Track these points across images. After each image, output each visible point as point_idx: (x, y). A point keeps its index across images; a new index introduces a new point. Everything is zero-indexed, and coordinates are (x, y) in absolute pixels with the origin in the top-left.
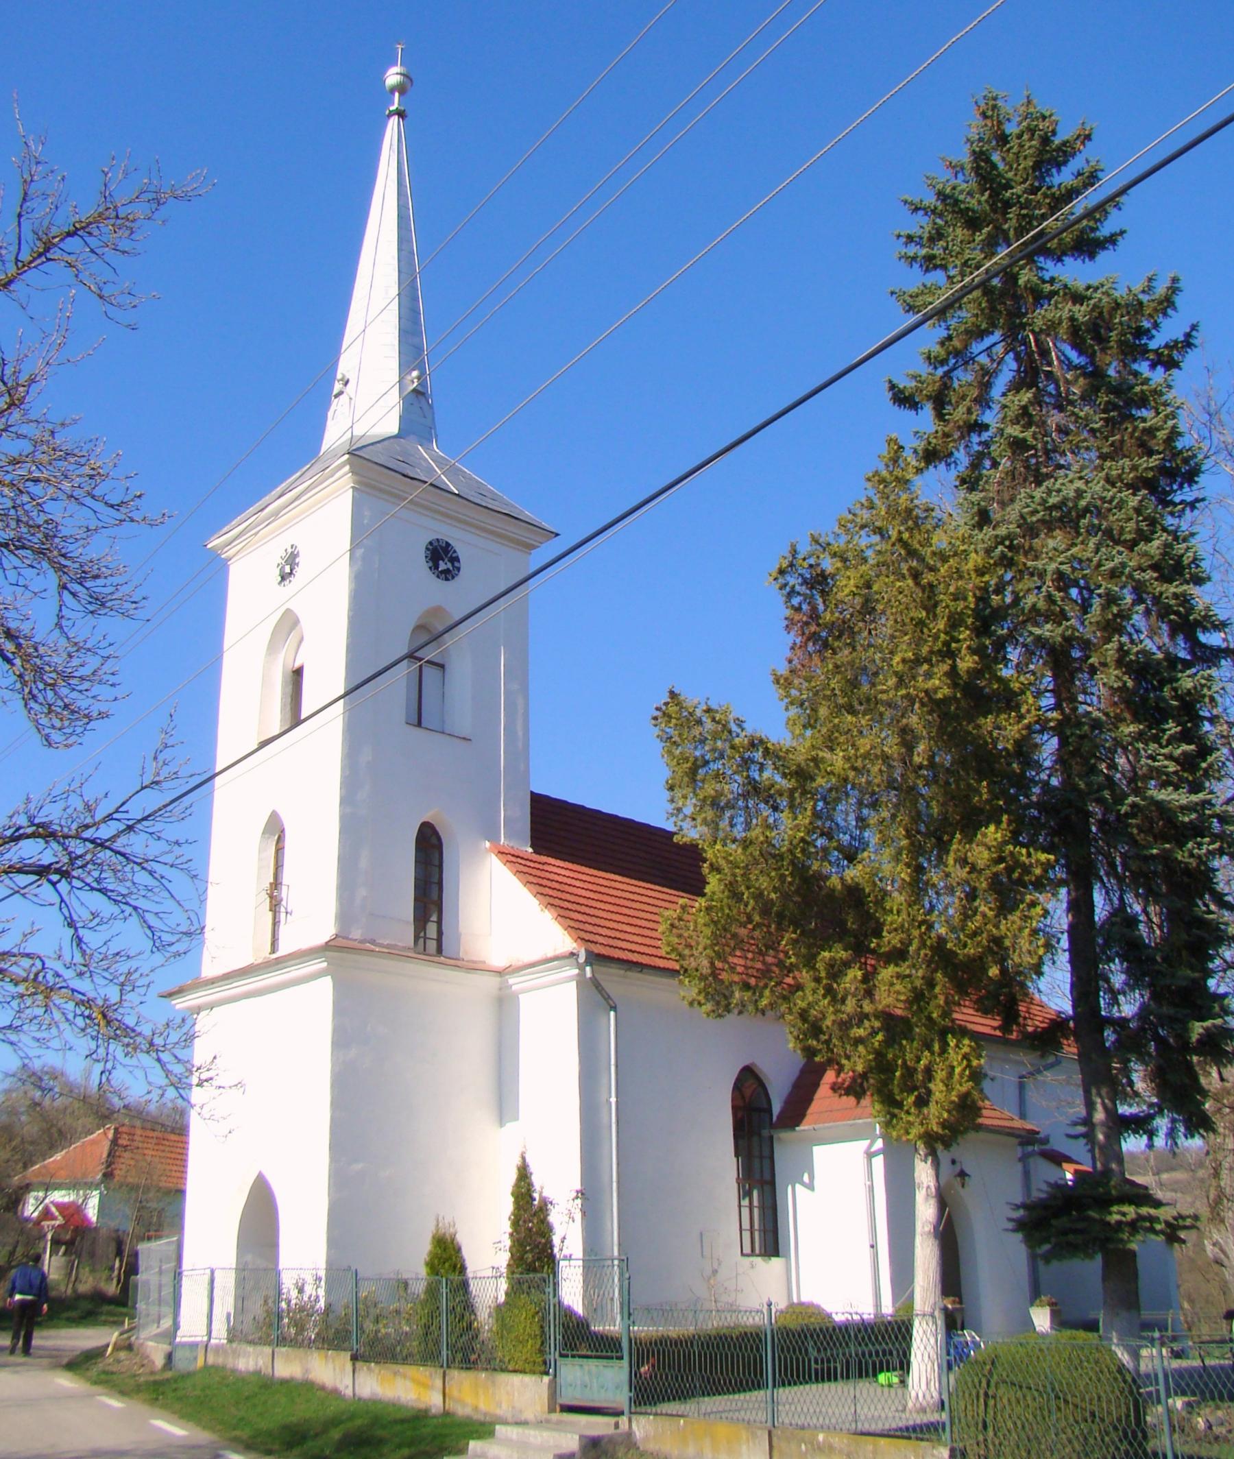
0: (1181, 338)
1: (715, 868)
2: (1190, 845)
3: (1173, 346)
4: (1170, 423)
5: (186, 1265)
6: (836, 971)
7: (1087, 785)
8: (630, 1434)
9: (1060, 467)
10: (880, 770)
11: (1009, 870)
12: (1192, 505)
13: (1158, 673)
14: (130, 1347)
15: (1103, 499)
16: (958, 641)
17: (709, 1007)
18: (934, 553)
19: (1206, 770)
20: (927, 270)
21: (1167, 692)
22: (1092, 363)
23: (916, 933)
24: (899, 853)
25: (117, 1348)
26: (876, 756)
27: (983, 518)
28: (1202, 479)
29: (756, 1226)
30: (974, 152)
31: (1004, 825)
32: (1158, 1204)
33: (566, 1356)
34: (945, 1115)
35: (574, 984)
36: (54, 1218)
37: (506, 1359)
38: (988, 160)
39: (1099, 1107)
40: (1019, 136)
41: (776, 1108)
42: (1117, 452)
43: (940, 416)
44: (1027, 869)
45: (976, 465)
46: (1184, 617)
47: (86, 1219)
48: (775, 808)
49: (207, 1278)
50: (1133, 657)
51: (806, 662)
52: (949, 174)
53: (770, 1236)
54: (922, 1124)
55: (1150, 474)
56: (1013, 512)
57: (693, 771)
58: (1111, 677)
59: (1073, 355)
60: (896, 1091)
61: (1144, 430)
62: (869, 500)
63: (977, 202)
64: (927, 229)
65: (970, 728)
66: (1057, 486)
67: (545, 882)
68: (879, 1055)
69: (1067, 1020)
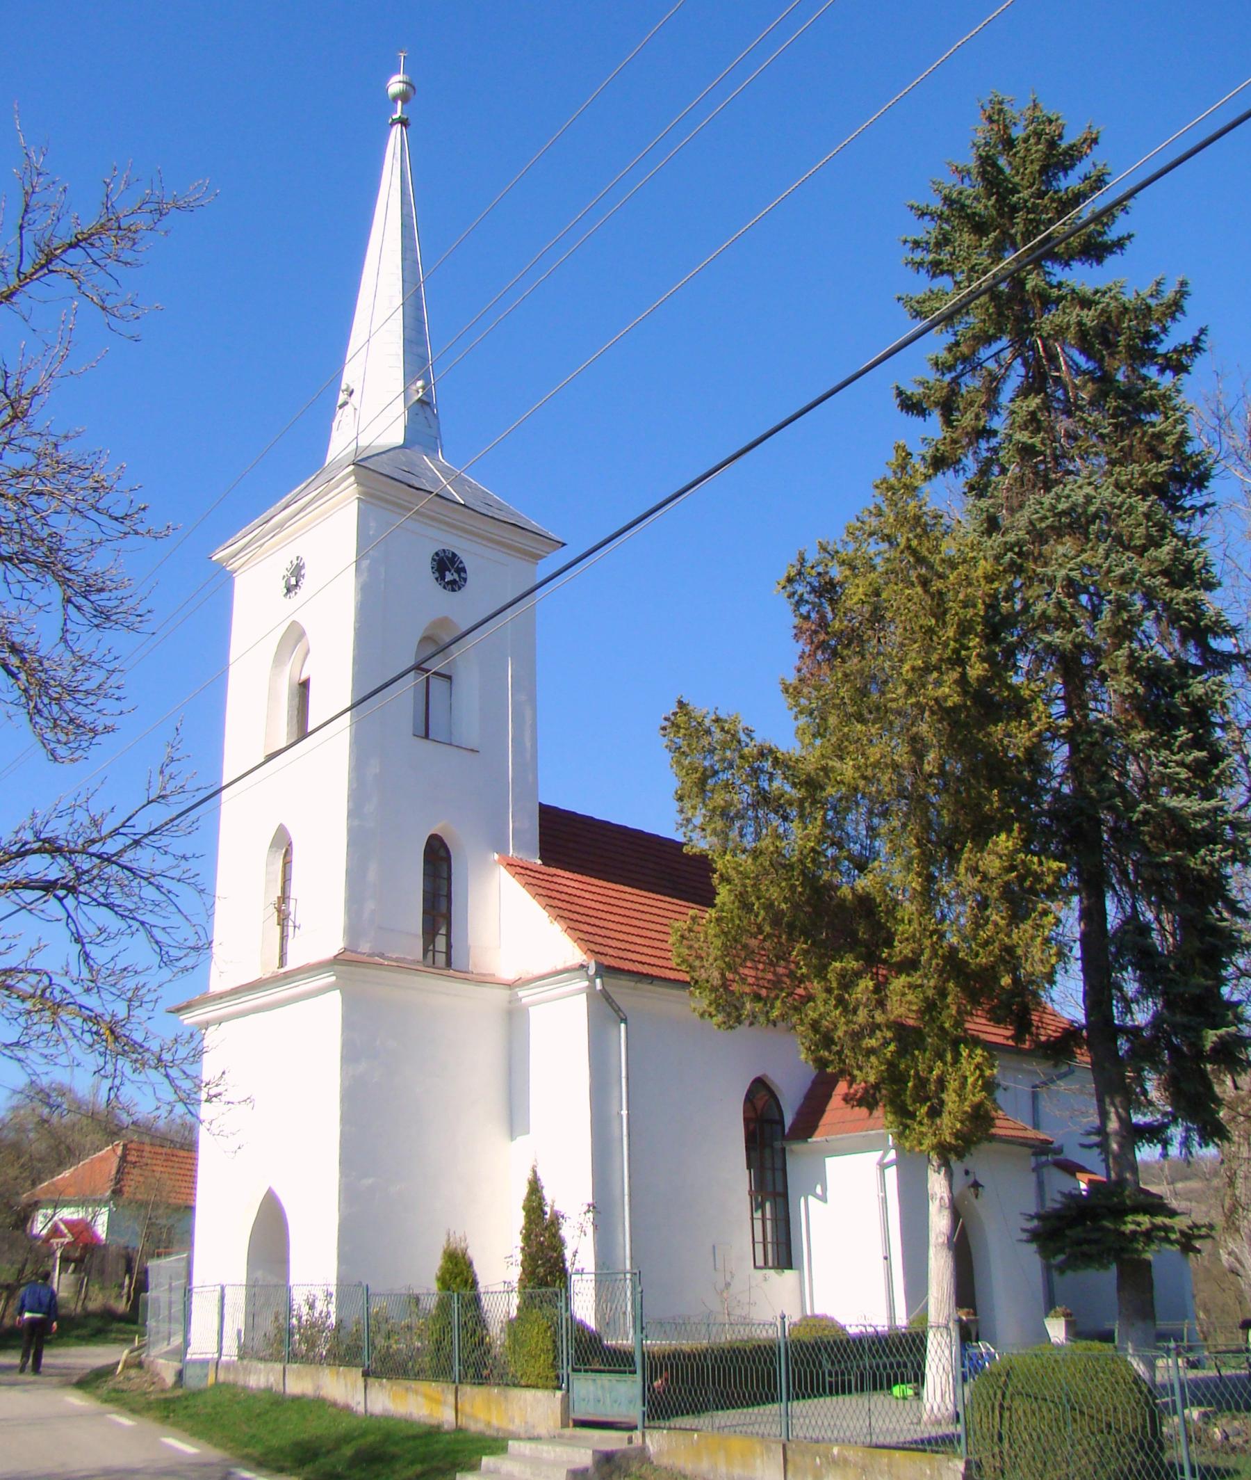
0: (1190, 342)
1: (725, 879)
2: (1202, 852)
3: (1182, 350)
4: (1179, 428)
5: (196, 1281)
6: (847, 981)
7: (1098, 792)
8: (643, 1448)
9: (1069, 473)
10: (890, 779)
11: (1021, 879)
12: (1202, 510)
13: (1169, 679)
14: (140, 1365)
15: (1112, 505)
16: (968, 648)
17: (719, 1018)
18: (943, 561)
19: (1218, 777)
20: (934, 276)
21: (1178, 696)
22: (1101, 368)
23: (927, 942)
24: (910, 862)
25: (127, 1365)
26: (887, 765)
27: (992, 525)
28: (1212, 484)
29: (769, 1239)
30: (980, 156)
31: (1015, 834)
32: (1172, 1213)
33: (579, 1371)
34: (958, 1125)
35: (584, 996)
36: (63, 1235)
37: (519, 1374)
38: (994, 165)
39: (1113, 1116)
40: (1026, 140)
41: (789, 1120)
42: (1126, 457)
43: (948, 422)
44: (1038, 878)
45: (984, 471)
46: (1195, 623)
47: (95, 1236)
48: (785, 818)
49: (217, 1295)
50: (1143, 664)
51: (815, 671)
52: (955, 179)
53: (783, 1248)
54: (935, 1135)
55: (1160, 480)
56: (1022, 518)
57: (702, 782)
58: (1122, 683)
59: (1081, 360)
60: (909, 1101)
61: (1153, 435)
62: (878, 507)
63: (984, 207)
64: (934, 235)
65: (980, 736)
66: (1066, 492)
67: (554, 894)
68: (891, 1065)
69: (1080, 1029)
